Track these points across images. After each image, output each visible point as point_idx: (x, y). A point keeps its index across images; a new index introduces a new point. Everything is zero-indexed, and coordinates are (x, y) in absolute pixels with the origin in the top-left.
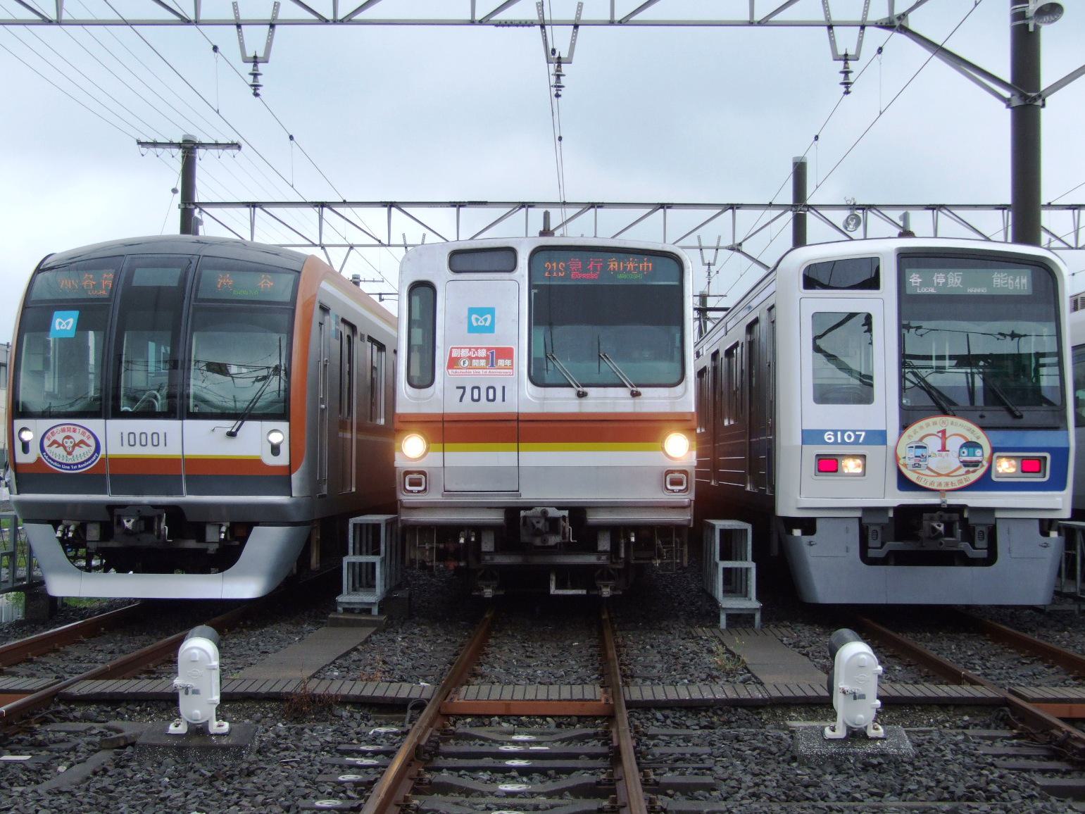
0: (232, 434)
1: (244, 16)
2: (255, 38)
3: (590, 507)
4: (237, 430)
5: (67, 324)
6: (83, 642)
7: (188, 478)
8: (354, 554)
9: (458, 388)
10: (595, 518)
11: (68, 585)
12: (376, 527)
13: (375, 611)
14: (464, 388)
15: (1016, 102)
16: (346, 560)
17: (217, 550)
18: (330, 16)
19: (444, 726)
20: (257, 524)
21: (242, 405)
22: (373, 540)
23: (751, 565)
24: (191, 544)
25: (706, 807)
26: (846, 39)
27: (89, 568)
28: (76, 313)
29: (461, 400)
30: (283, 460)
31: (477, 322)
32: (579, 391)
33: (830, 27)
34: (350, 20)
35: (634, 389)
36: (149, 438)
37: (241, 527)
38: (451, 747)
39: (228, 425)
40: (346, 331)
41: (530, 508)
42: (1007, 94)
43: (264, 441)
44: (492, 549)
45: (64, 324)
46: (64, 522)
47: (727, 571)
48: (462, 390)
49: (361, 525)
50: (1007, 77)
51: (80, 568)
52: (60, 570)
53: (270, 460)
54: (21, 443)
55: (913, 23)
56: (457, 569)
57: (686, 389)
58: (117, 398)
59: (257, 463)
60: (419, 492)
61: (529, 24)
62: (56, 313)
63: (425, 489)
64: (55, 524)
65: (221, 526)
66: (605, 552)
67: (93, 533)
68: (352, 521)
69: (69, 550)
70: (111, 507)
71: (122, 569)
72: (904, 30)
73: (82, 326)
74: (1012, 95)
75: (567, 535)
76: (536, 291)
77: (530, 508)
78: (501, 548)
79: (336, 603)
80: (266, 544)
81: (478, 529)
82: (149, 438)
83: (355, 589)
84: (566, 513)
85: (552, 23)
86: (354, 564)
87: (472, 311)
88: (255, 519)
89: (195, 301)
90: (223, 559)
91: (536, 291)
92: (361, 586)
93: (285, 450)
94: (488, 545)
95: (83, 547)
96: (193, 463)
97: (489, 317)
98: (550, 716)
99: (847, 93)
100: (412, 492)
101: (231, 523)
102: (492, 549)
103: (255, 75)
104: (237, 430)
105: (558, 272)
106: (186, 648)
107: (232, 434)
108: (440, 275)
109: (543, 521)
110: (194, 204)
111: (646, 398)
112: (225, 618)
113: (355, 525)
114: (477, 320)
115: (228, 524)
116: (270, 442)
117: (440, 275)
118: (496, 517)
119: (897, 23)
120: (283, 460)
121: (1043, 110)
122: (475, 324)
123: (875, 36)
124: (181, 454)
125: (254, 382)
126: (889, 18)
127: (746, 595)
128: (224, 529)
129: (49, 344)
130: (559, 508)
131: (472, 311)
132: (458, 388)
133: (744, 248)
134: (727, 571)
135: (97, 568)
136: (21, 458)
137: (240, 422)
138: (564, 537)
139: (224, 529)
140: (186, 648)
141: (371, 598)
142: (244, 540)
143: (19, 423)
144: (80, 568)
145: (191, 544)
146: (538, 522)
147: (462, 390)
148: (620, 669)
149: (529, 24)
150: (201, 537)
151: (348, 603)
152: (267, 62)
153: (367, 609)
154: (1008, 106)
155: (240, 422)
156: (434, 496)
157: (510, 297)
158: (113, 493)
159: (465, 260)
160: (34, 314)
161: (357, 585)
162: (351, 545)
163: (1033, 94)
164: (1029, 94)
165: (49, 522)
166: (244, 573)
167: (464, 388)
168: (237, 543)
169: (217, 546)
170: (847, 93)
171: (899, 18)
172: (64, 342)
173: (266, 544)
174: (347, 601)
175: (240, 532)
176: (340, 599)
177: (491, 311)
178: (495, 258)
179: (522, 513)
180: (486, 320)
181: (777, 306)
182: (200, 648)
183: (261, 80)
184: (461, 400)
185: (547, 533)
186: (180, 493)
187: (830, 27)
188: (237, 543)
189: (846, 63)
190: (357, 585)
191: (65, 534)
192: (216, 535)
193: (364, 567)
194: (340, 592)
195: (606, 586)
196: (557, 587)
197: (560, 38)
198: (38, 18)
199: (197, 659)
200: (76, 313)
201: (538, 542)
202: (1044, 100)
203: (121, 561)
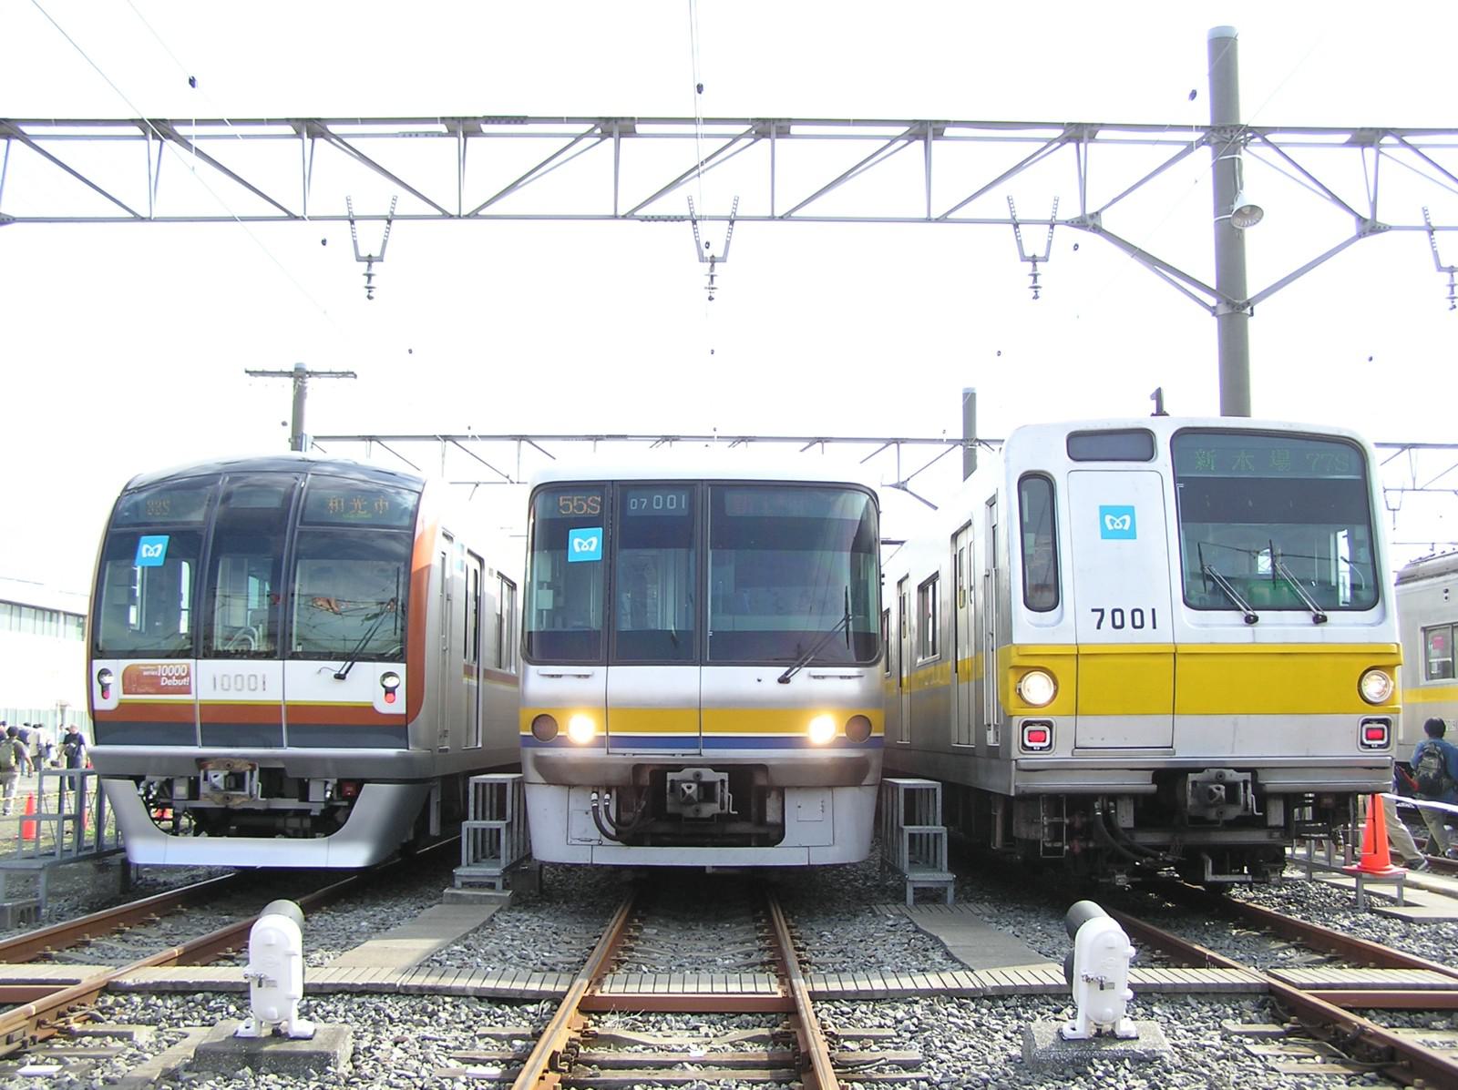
0: (340, 677)
1: (356, 212)
2: (370, 235)
3: (1263, 768)
4: (347, 672)
5: (156, 550)
6: (181, 913)
7: (289, 726)
8: (476, 819)
9: (1093, 610)
10: (1274, 782)
11: (155, 850)
12: (502, 787)
13: (499, 883)
14: (1102, 611)
15: (1222, 310)
16: (465, 825)
17: (323, 811)
18: (454, 212)
19: (585, 1026)
20: (369, 781)
21: (350, 646)
22: (498, 804)
23: (940, 829)
24: (292, 804)
25: (352, 1089)
26: (1034, 239)
27: (175, 830)
28: (166, 538)
29: (1099, 627)
30: (399, 706)
31: (1113, 525)
32: (1318, 615)
33: (1016, 226)
34: (477, 215)
35: (1251, 613)
36: (232, 684)
37: (349, 788)
38: (601, 1053)
39: (337, 666)
40: (475, 565)
41: (1200, 770)
42: (1212, 301)
43: (368, 686)
44: (1132, 825)
45: (152, 550)
46: (147, 777)
47: (912, 836)
48: (1099, 613)
49: (484, 785)
50: (1213, 284)
51: (166, 831)
52: (145, 833)
53: (384, 707)
54: (100, 686)
55: (1107, 222)
56: (1086, 851)
57: (1384, 614)
58: (209, 637)
59: (370, 709)
60: (1041, 749)
61: (682, 219)
62: (144, 538)
63: (1050, 745)
64: (138, 780)
65: (326, 783)
66: (1277, 828)
67: (181, 790)
68: (474, 779)
69: (153, 810)
70: (201, 762)
71: (214, 833)
72: (1097, 229)
73: (172, 556)
74: (1218, 303)
75: (1250, 807)
76: (1182, 485)
77: (1200, 770)
78: (1141, 823)
79: (452, 876)
80: (375, 802)
81: (1114, 797)
82: (232, 684)
83: (476, 861)
84: (725, 776)
85: (702, 218)
86: (475, 830)
87: (1104, 511)
88: (366, 776)
89: (302, 523)
90: (327, 824)
91: (1182, 485)
92: (484, 857)
93: (401, 693)
94: (1126, 819)
95: (170, 808)
96: (295, 709)
97: (1127, 518)
98: (671, 1013)
99: (1036, 297)
100: (1032, 749)
101: (339, 780)
102: (1132, 825)
103: (369, 276)
104: (347, 672)
105: (1206, 466)
106: (259, 928)
107: (340, 677)
108: (1057, 463)
109: (694, 786)
110: (977, 440)
111: (1331, 624)
112: (320, 892)
113: (476, 785)
114: (1112, 522)
115: (335, 781)
116: (384, 686)
117: (1057, 463)
118: (1143, 784)
119: (1090, 223)
120: (399, 706)
121: (1250, 320)
122: (1110, 527)
123: (1066, 235)
124: (281, 699)
125: (363, 621)
126: (1081, 217)
127: (935, 866)
128: (329, 787)
129: (135, 576)
130: (1239, 770)
131: (1104, 511)
132: (1093, 610)
133: (909, 486)
134: (912, 836)
135: (186, 831)
136: (101, 704)
137: (349, 663)
138: (722, 808)
139: (329, 787)
140: (259, 928)
141: (492, 870)
142: (352, 800)
143: (99, 664)
144: (166, 831)
145: (292, 804)
146: (689, 788)
147: (1099, 613)
148: (801, 968)
149: (682, 219)
150: (304, 796)
151: (467, 876)
152: (382, 261)
153: (491, 883)
154: (1214, 314)
155: (349, 663)
156: (1062, 753)
157: (1151, 489)
158: (204, 745)
159: (1089, 445)
160: (119, 543)
161: (480, 856)
162: (471, 809)
163: (1241, 302)
164: (1237, 301)
165: (131, 778)
166: (350, 838)
167: (1102, 611)
168: (345, 803)
169: (323, 806)
170: (1036, 297)
171: (1092, 216)
172: (151, 571)
173: (375, 802)
174: (467, 874)
175: (349, 790)
176: (457, 871)
177: (1130, 510)
178: (1128, 444)
179: (670, 776)
180: (1124, 522)
181: (905, 544)
182: (279, 926)
183: (374, 282)
184: (1099, 627)
185: (700, 801)
186: (281, 746)
187: (1016, 226)
188: (345, 803)
189: (1035, 265)
190: (480, 856)
191: (148, 792)
192: (319, 795)
193: (480, 832)
194: (459, 864)
195: (1121, 871)
196: (1214, 873)
197: (714, 233)
198: (131, 215)
199: (273, 942)
200: (166, 538)
201: (1212, 814)
202: (1252, 309)
203: (214, 823)
